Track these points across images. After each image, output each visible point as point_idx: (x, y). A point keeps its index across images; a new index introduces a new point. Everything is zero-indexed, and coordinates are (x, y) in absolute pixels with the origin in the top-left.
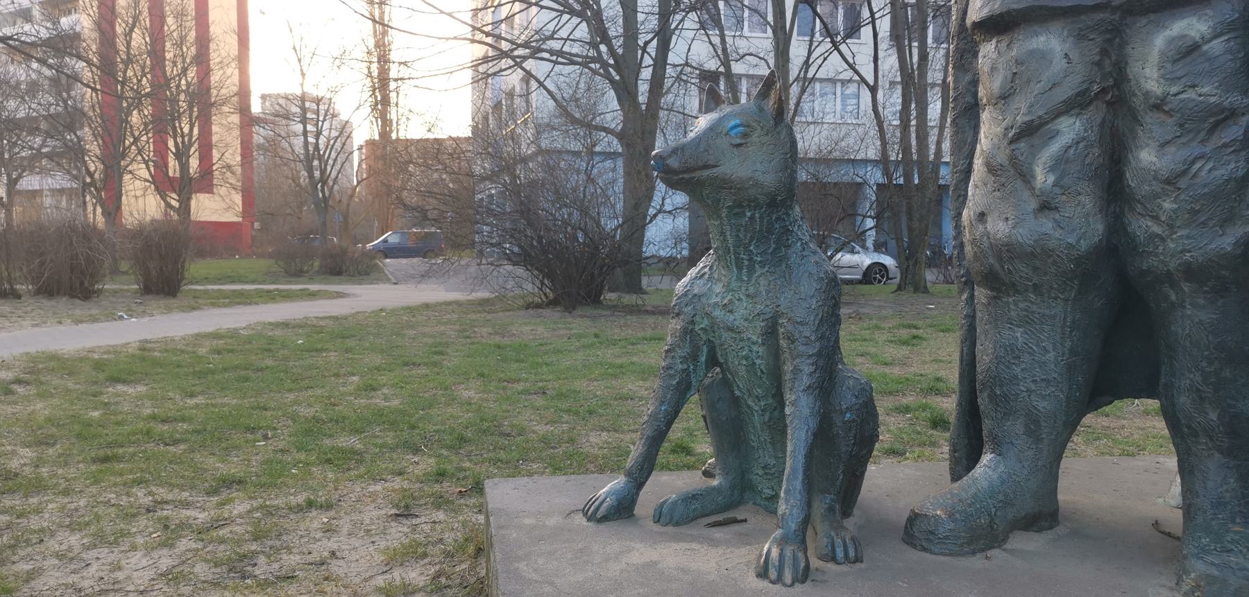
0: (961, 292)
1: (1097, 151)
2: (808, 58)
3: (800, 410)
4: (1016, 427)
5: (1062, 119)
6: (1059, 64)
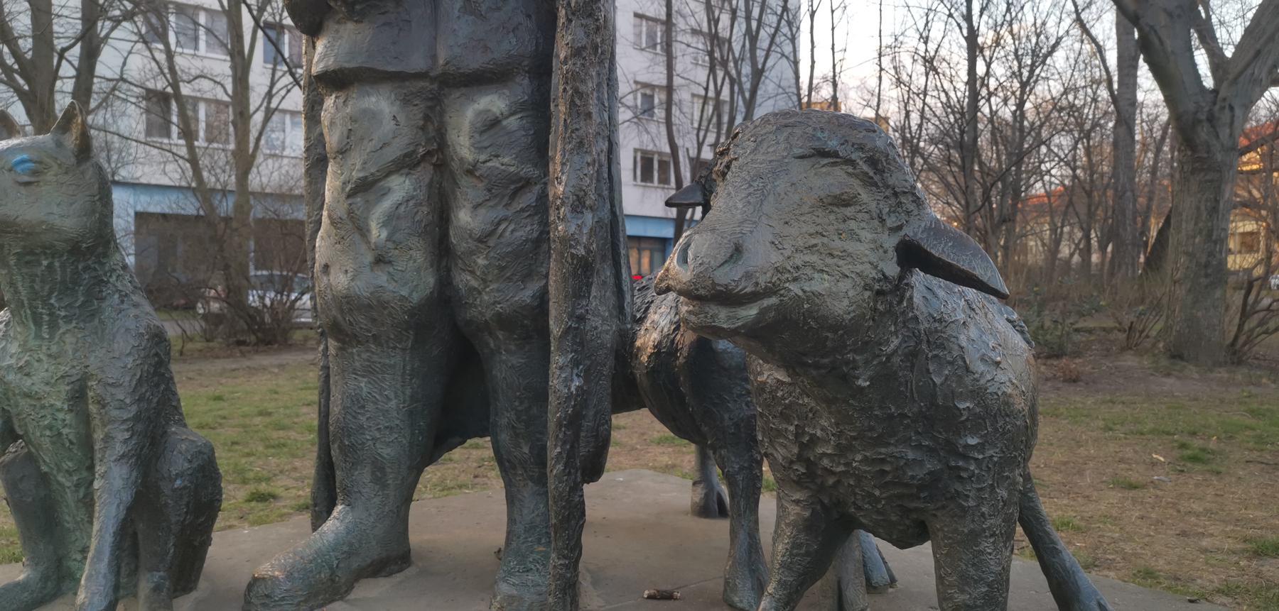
0: (319, 343)
1: (425, 209)
2: (271, 87)
3: (112, 485)
4: (364, 475)
5: (393, 177)
6: (388, 125)
